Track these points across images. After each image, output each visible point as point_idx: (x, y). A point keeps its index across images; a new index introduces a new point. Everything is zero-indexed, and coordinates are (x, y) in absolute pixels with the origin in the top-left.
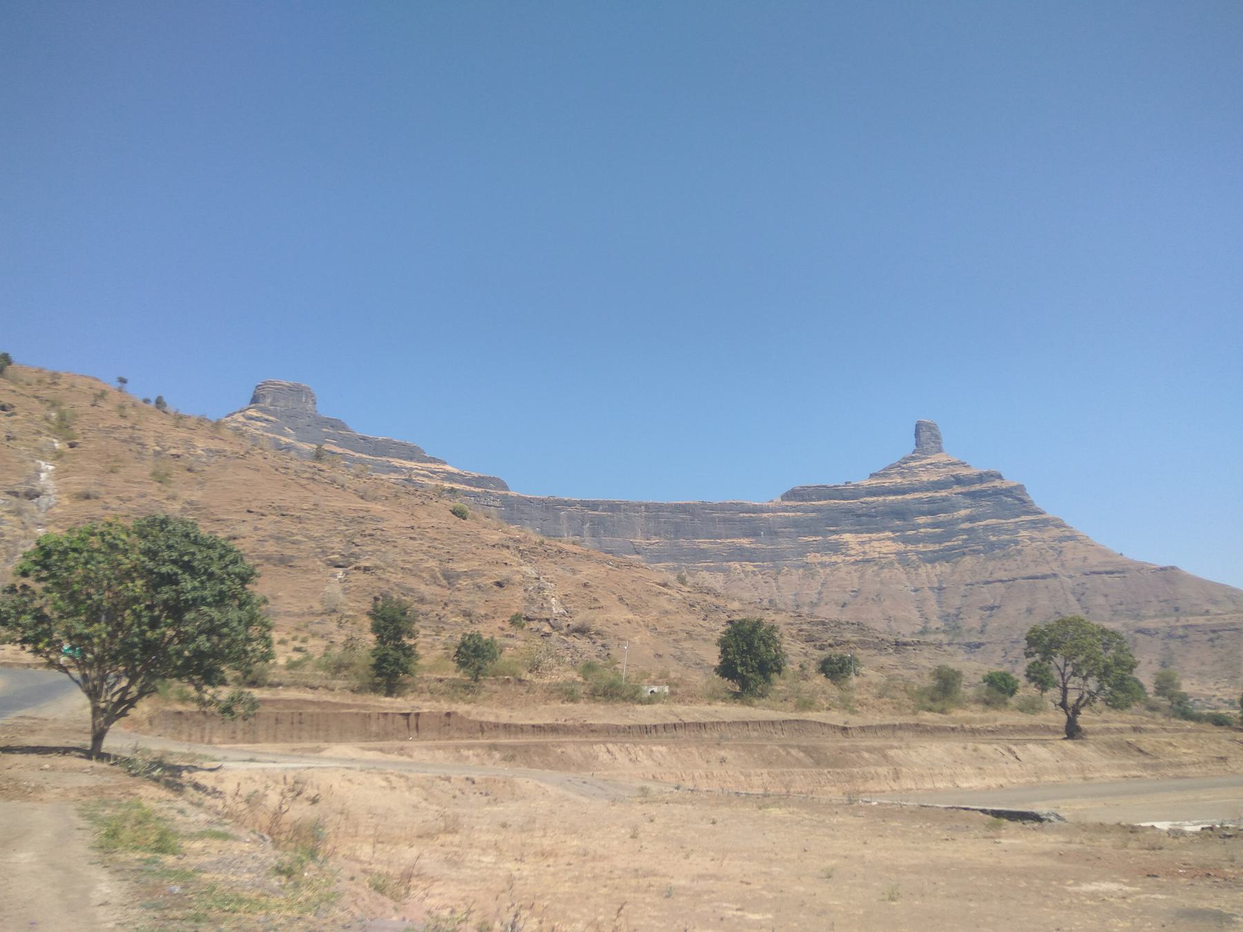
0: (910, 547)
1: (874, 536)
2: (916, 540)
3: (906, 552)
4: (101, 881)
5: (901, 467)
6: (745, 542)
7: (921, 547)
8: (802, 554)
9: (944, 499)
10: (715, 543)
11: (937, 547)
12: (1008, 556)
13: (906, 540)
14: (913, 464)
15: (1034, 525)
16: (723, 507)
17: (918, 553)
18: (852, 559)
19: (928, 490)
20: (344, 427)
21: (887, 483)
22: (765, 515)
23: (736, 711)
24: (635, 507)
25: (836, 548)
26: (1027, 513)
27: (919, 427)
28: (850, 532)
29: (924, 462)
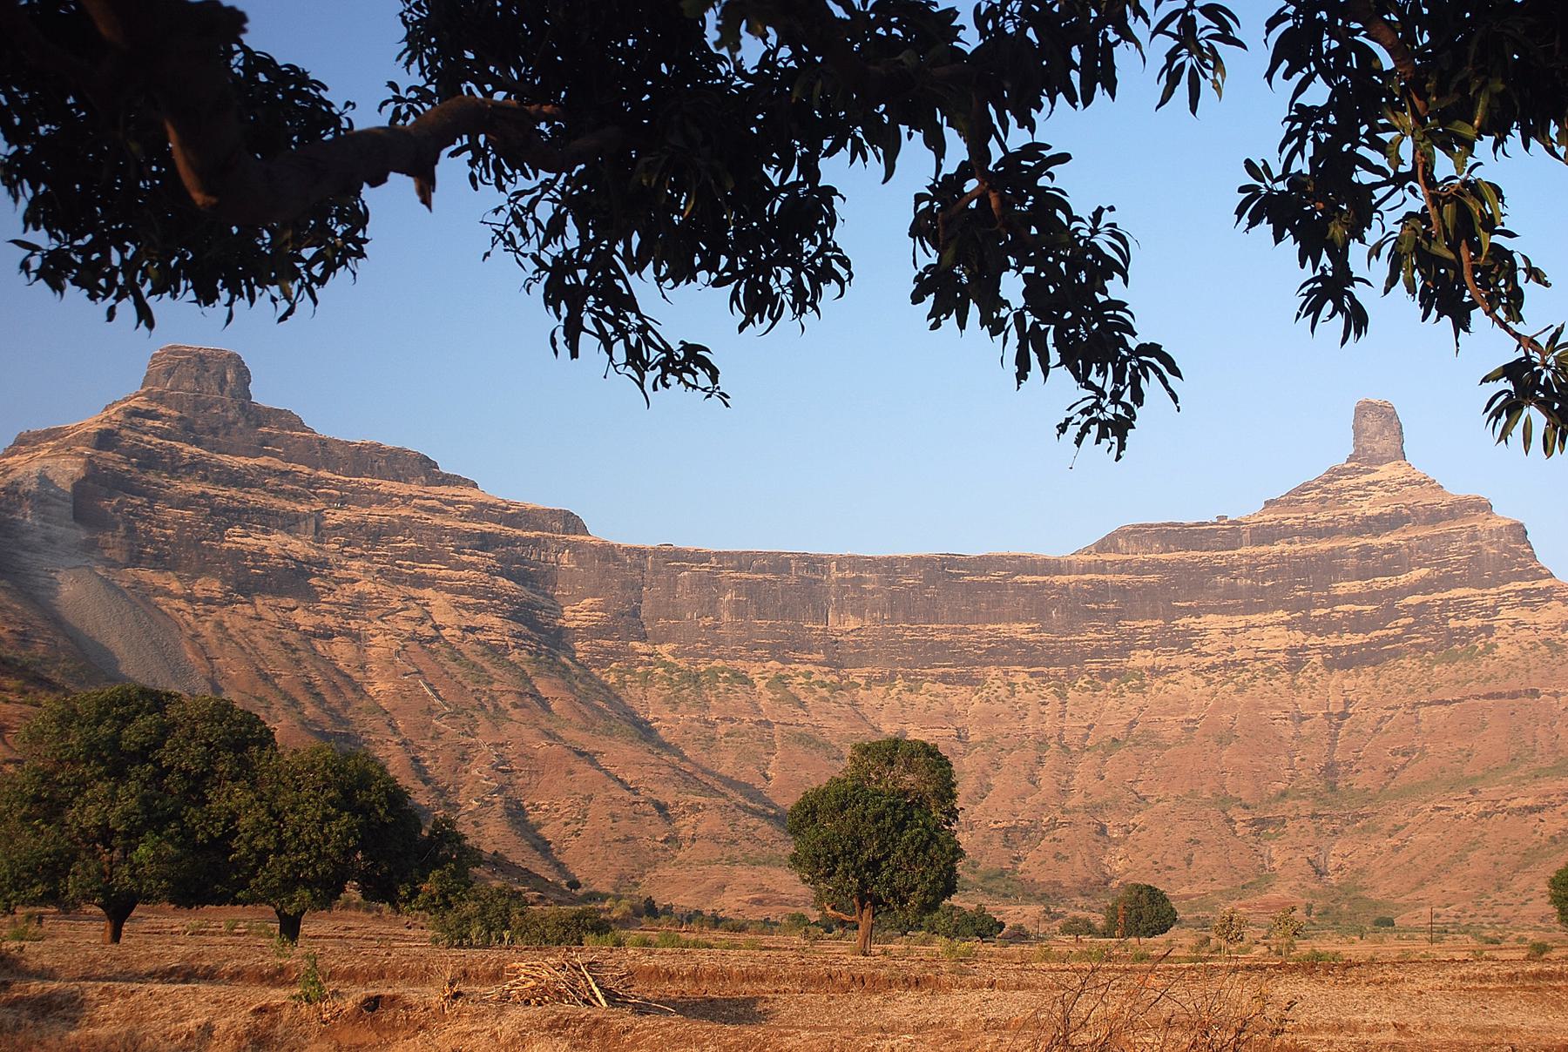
0: (1314, 640)
1: (1255, 618)
2: (1327, 626)
3: (1304, 648)
4: (937, 145)
5: (1327, 488)
6: (1020, 630)
7: (1332, 641)
8: (1124, 651)
9: (1390, 549)
10: (1104, 663)
11: (1359, 639)
12: (1471, 655)
13: (1307, 626)
14: (1344, 482)
15: (1528, 599)
16: (985, 563)
17: (1325, 649)
18: (1208, 661)
19: (1358, 533)
20: (297, 424)
21: (1292, 518)
22: (1063, 579)
23: (904, 710)
24: (832, 558)
25: (1184, 641)
26: (1520, 577)
27: (1363, 410)
28: (1213, 610)
29: (1364, 479)
